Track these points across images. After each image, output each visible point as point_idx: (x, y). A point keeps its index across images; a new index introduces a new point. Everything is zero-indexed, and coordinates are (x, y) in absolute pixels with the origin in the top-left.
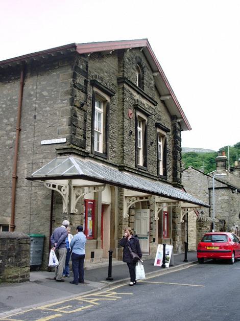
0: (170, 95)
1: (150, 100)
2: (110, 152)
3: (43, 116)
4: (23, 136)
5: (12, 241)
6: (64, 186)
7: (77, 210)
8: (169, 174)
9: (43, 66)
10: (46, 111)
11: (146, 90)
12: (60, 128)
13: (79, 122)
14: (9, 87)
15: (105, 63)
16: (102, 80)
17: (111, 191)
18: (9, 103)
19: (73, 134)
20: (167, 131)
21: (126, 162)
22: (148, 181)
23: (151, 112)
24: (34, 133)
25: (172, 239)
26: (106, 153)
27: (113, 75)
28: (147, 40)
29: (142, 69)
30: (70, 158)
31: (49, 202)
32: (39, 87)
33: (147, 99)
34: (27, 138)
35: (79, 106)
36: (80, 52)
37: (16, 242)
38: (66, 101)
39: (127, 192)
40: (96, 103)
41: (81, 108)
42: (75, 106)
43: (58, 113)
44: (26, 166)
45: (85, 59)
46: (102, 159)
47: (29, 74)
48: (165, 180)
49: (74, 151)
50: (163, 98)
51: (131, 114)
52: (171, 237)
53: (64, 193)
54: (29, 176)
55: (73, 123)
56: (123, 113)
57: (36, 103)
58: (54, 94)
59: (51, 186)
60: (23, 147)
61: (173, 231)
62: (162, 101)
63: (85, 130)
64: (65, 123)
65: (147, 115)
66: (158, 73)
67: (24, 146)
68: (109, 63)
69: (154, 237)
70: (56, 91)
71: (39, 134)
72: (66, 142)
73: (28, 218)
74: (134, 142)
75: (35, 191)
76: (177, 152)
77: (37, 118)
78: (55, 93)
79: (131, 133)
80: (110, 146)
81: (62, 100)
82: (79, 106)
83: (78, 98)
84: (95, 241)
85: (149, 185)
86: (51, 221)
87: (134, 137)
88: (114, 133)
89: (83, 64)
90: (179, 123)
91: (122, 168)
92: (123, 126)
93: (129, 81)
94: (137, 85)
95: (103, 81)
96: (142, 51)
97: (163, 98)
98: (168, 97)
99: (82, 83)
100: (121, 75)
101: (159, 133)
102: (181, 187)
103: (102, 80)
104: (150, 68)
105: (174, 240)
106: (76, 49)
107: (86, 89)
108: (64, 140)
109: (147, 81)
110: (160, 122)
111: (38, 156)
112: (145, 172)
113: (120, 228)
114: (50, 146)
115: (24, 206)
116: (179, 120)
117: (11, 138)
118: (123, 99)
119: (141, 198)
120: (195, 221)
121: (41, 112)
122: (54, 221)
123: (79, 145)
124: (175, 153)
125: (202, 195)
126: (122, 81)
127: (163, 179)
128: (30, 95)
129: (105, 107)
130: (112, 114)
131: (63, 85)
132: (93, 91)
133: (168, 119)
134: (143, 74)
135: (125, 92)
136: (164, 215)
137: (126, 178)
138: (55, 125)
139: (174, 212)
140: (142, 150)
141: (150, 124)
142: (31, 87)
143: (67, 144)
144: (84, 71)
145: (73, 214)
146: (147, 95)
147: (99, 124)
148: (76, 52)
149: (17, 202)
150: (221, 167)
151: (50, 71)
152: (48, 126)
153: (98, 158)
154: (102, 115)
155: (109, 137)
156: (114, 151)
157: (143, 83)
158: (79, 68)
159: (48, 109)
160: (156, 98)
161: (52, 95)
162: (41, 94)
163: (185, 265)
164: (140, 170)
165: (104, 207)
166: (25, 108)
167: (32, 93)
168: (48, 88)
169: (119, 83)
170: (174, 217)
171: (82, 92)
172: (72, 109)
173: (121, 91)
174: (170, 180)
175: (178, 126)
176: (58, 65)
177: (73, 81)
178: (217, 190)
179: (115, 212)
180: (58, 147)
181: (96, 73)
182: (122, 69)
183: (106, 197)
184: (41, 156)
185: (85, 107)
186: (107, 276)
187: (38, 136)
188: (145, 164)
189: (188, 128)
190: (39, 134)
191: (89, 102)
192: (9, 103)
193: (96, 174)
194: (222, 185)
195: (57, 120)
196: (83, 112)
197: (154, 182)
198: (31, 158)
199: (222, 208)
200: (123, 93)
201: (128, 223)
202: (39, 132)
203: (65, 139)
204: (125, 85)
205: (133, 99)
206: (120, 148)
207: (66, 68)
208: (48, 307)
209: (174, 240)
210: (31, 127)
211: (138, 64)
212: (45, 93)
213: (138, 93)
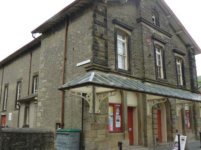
0: (182, 30)
2: (133, 69)
3: (78, 47)
4: (68, 63)
5: (37, 135)
6: (89, 94)
7: (100, 111)
8: (188, 84)
10: (79, 44)
11: (161, 27)
13: (100, 47)
14: (60, 33)
17: (137, 97)
18: (61, 43)
19: (95, 55)
20: (183, 55)
21: (147, 76)
22: (167, 88)
26: (130, 70)
27: (133, 18)
29: (157, 13)
32: (75, 29)
33: (163, 33)
34: (70, 63)
37: (40, 136)
39: (149, 97)
40: (156, 49)
41: (101, 37)
42: (95, 36)
46: (126, 74)
48: (184, 88)
49: (96, 68)
51: (149, 42)
52: (193, 128)
53: (89, 99)
54: (60, 88)
55: (95, 47)
56: (142, 42)
59: (82, 94)
61: (194, 125)
62: (177, 35)
63: (106, 52)
64: (90, 49)
65: (164, 44)
66: (170, 16)
68: (129, 9)
69: (176, 129)
72: (90, 62)
74: (154, 61)
77: (75, 49)
81: (88, 34)
84: (122, 133)
87: (153, 58)
88: (136, 56)
90: (192, 49)
91: (144, 80)
92: (143, 51)
93: (145, 20)
97: (177, 33)
100: (139, 17)
101: (177, 56)
102: (198, 93)
104: (163, 13)
105: (196, 131)
108: (89, 61)
109: (162, 21)
110: (176, 49)
112: (164, 82)
116: (192, 47)
117: (61, 65)
118: (142, 32)
119: (159, 100)
121: (76, 45)
127: (184, 88)
128: (71, 35)
129: (128, 39)
130: (133, 43)
132: (115, 27)
133: (184, 47)
134: (159, 16)
135: (143, 27)
136: (186, 113)
137: (148, 87)
139: (194, 111)
140: (162, 67)
141: (167, 50)
142: (71, 30)
143: (91, 63)
144: (103, 13)
145: (97, 114)
146: (163, 30)
147: (121, 50)
149: (65, 107)
153: (121, 73)
154: (126, 44)
156: (137, 69)
157: (159, 22)
158: (99, 11)
160: (171, 32)
162: (77, 33)
164: (160, 81)
165: (131, 109)
166: (68, 44)
167: (72, 33)
169: (138, 22)
170: (195, 114)
171: (102, 26)
172: (94, 38)
173: (140, 27)
174: (189, 88)
175: (191, 51)
177: (94, 19)
179: (141, 111)
181: (117, 16)
182: (139, 13)
183: (131, 100)
187: (75, 61)
188: (165, 77)
192: (61, 43)
193: (100, 81)
196: (104, 41)
197: (174, 89)
200: (141, 29)
201: (151, 120)
204: (142, 23)
206: (142, 66)
209: (196, 131)
211: (153, 10)
212: (79, 32)
213: (155, 29)
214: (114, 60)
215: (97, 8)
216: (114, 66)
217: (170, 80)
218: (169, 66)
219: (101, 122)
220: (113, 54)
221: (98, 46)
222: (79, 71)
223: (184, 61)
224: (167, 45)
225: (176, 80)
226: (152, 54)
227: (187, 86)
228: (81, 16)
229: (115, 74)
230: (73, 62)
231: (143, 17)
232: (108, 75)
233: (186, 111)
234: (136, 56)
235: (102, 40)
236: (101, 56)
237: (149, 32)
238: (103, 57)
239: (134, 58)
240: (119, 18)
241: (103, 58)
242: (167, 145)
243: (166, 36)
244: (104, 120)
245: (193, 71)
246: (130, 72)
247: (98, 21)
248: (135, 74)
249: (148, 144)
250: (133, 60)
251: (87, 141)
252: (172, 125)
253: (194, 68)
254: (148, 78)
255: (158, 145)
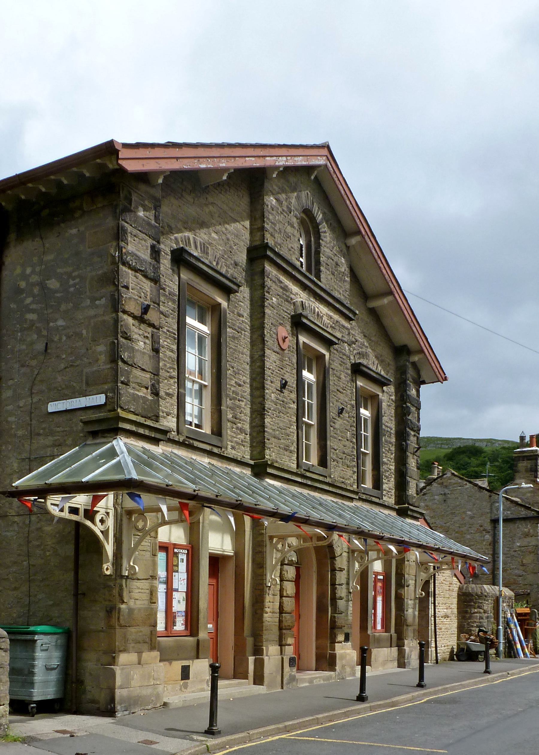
0: (391, 293)
1: (338, 306)
8: (389, 485)
9: (45, 212)
10: (57, 328)
11: (326, 280)
12: (87, 370)
15: (211, 207)
16: (205, 251)
23: (339, 335)
24: (33, 384)
25: (395, 636)
28: (328, 147)
30: (114, 442)
31: (69, 550)
35: (138, 313)
36: (131, 166)
38: (103, 301)
43: (84, 332)
44: (15, 465)
45: (152, 191)
46: (208, 448)
47: (12, 236)
48: (377, 500)
50: (373, 304)
57: (33, 311)
58: (74, 285)
59: (66, 510)
60: (7, 422)
63: (156, 374)
64: (103, 358)
67: (10, 419)
68: (225, 207)
70: (78, 276)
71: (44, 387)
73: (25, 588)
75: (39, 525)
76: (409, 435)
78: (77, 280)
79: (284, 385)
80: (230, 416)
81: (94, 299)
82: (138, 313)
83: (132, 293)
85: (366, 517)
86: (76, 595)
87: (294, 396)
88: (240, 385)
89: (147, 203)
90: (414, 364)
94: (304, 269)
95: (207, 253)
96: (316, 177)
97: (373, 304)
98: (386, 301)
99: (146, 255)
103: (205, 251)
106: (118, 158)
107: (156, 269)
109: (329, 257)
110: (364, 362)
111: (43, 441)
113: (259, 611)
114: (69, 416)
115: (15, 563)
116: (415, 358)
120: (455, 594)
122: (84, 594)
123: (140, 411)
124: (402, 436)
125: (477, 536)
126: (259, 253)
128: (19, 291)
130: (234, 338)
131: (96, 259)
136: (376, 581)
137: (274, 493)
138: (78, 363)
141: (336, 365)
142: (18, 270)
144: (149, 224)
148: (122, 171)
150: (526, 471)
151: (62, 225)
152: (62, 366)
153: (196, 444)
155: (227, 396)
159: (61, 323)
161: (70, 287)
162: (42, 286)
163: (418, 696)
164: (308, 474)
165: (216, 561)
167: (23, 284)
168: (59, 270)
171: (146, 276)
174: (390, 499)
176: (81, 208)
178: (511, 526)
180: (85, 417)
184: (49, 441)
185: (152, 316)
186: (358, 692)
187: (41, 392)
188: (323, 462)
189: (440, 377)
190: (44, 387)
191: (169, 306)
194: (523, 513)
195: (83, 351)
196: (150, 330)
198: (27, 446)
199: (523, 565)
201: (278, 597)
202: (42, 381)
203: (103, 396)
205: (289, 300)
207: (101, 215)
208: (301, 735)
210: (23, 370)
212: (53, 284)
213: (304, 287)
214: (175, 398)
215: (131, 204)
216: (175, 420)
217: (341, 472)
218: (339, 423)
219: (138, 602)
220: (171, 377)
221: (133, 348)
222: (58, 429)
223: (384, 405)
224: (336, 346)
225: (354, 472)
226: (292, 381)
227: (384, 493)
228: (63, 221)
229: (176, 448)
230: (32, 393)
231: (270, 241)
232: (161, 451)
233: (377, 574)
234: (240, 385)
235: (143, 326)
236: (140, 385)
237: (287, 301)
238: (147, 388)
239: (233, 392)
240: (195, 243)
241: (144, 390)
242: (316, 678)
243: (336, 317)
244: (146, 596)
245: (409, 442)
246: (222, 441)
247: (133, 254)
248: (233, 448)
249: (265, 675)
250: (231, 400)
251: (89, 663)
252: (333, 618)
253: (412, 433)
254: (276, 464)
255: (293, 679)
